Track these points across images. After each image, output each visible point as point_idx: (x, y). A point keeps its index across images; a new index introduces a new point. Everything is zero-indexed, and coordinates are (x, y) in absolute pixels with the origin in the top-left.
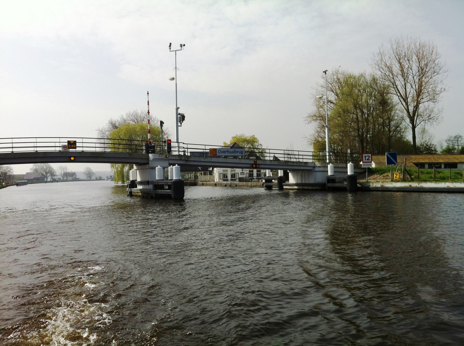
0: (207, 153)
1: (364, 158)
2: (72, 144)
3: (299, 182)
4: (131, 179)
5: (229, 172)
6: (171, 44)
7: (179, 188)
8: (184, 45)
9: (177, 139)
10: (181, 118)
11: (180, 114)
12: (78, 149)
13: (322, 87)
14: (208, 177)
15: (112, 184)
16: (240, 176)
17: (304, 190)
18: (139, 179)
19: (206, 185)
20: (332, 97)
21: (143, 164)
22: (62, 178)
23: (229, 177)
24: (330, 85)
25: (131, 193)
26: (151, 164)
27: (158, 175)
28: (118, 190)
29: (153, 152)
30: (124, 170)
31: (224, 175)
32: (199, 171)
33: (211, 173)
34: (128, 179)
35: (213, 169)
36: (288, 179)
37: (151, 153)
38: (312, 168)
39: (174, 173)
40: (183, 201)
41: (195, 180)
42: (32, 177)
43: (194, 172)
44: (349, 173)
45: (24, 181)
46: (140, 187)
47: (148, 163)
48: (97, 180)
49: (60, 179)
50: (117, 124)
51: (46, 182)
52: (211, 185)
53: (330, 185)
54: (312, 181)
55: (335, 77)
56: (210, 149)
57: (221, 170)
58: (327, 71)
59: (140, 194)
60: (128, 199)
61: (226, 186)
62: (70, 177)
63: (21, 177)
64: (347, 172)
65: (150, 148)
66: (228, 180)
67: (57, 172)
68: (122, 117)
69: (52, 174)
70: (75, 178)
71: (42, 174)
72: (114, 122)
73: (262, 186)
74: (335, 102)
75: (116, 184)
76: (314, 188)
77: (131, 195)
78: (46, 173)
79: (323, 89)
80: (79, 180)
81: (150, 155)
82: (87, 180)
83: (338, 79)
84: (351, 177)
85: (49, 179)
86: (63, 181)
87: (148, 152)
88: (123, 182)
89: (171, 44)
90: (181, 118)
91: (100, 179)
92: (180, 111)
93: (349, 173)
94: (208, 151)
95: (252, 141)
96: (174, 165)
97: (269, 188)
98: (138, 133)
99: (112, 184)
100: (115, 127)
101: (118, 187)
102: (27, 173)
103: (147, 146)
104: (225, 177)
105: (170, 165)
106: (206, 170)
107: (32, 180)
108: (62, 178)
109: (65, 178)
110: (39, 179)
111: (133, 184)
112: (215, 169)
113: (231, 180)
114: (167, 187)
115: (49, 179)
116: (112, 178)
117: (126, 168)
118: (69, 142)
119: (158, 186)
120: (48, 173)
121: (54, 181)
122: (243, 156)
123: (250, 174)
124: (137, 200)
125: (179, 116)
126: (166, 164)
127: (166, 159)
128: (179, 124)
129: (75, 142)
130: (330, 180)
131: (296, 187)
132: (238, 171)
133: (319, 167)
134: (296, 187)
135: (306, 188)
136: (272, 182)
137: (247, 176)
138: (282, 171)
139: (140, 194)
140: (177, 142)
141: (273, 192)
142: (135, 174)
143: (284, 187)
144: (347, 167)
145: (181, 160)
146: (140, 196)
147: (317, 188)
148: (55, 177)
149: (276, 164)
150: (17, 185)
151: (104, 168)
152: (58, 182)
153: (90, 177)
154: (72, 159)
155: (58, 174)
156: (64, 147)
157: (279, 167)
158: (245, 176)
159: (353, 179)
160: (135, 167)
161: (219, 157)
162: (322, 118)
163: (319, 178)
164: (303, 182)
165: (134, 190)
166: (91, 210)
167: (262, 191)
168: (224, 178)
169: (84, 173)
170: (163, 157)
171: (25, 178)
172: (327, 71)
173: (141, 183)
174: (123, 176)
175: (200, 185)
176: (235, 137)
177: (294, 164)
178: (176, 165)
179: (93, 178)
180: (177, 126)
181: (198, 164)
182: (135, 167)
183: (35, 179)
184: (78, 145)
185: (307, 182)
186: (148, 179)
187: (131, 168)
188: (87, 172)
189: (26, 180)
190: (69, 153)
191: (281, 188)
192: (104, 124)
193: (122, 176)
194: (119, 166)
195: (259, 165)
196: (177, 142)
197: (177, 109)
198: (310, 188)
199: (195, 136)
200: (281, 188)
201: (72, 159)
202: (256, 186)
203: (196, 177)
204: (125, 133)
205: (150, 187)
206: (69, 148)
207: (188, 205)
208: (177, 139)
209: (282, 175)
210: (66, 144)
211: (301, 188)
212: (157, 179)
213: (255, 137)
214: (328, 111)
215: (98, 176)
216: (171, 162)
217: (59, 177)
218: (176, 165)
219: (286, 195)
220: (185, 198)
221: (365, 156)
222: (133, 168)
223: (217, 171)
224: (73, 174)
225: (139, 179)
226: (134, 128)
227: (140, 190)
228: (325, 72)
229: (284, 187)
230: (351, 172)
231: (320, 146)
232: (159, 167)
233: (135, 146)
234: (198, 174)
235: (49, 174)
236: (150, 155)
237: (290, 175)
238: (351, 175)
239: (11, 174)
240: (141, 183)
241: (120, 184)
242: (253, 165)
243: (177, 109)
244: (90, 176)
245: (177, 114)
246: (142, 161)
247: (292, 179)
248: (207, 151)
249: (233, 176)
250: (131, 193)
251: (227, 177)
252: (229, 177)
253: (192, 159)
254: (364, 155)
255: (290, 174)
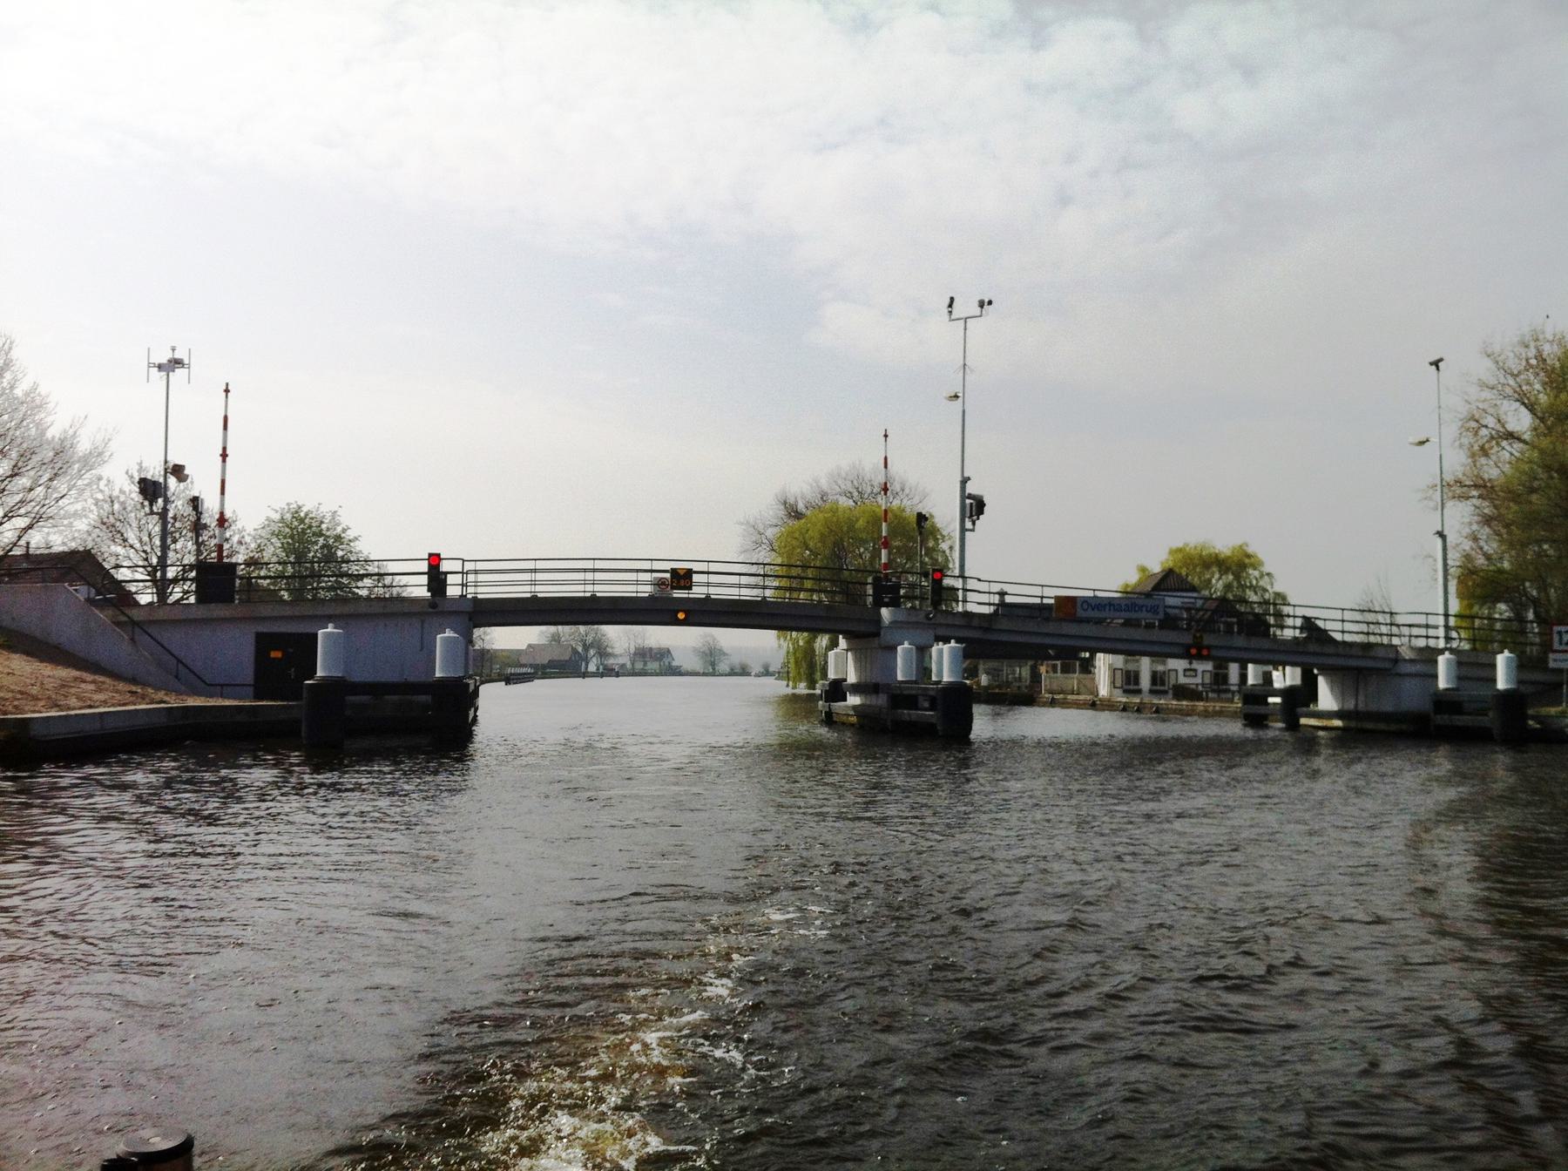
0: (1049, 607)
1: (1556, 638)
2: (682, 578)
3: (1350, 705)
4: (832, 675)
5: (1145, 666)
6: (952, 299)
7: (955, 706)
8: (990, 303)
9: (962, 566)
10: (974, 507)
11: (970, 496)
12: (698, 592)
13: (1483, 385)
14: (1074, 680)
15: (782, 688)
16: (1182, 680)
17: (1365, 733)
18: (852, 678)
19: (1065, 704)
20: (1521, 421)
21: (867, 637)
22: (629, 665)
23: (1145, 682)
24: (1511, 382)
25: (829, 714)
26: (887, 638)
27: (902, 670)
28: (796, 706)
29: (894, 603)
30: (817, 645)
31: (1128, 673)
32: (1049, 658)
33: (1087, 667)
34: (825, 675)
35: (1092, 657)
36: (1314, 697)
37: (887, 605)
38: (1387, 665)
39: (945, 662)
40: (969, 743)
41: (1030, 687)
42: (543, 659)
43: (1030, 663)
44: (1501, 685)
45: (524, 670)
46: (854, 700)
47: (877, 635)
48: (732, 673)
49: (623, 666)
50: (801, 507)
51: (585, 675)
52: (1078, 705)
53: (1442, 719)
54: (1388, 706)
55: (1532, 352)
56: (1057, 598)
57: (1118, 660)
58: (1441, 360)
59: (854, 719)
60: (822, 731)
61: (1124, 710)
62: (656, 663)
63: (513, 657)
64: (1494, 681)
65: (887, 592)
66: (1139, 692)
67: (617, 645)
68: (817, 481)
69: (603, 653)
70: (670, 666)
71: (575, 651)
72: (792, 501)
73: (1233, 715)
74: (1526, 437)
75: (790, 691)
76: (1393, 727)
77: (829, 720)
78: (586, 648)
79: (1487, 394)
80: (681, 674)
81: (885, 612)
82: (704, 674)
83: (1540, 357)
84: (1506, 694)
85: (592, 668)
86: (634, 673)
87: (879, 603)
88: (812, 685)
89: (952, 299)
90: (974, 507)
91: (744, 672)
92: (971, 488)
93: (1501, 685)
94: (1052, 601)
95: (1239, 565)
96: (946, 640)
97: (1256, 722)
98: (864, 536)
99: (782, 688)
100: (794, 513)
101: (795, 698)
102: (530, 646)
103: (877, 584)
104: (1129, 681)
105: (938, 639)
106: (1075, 659)
107: (544, 667)
108: (629, 665)
109: (639, 666)
110: (566, 667)
111: (837, 690)
112: (1100, 656)
113: (1151, 692)
114: (926, 705)
115: (592, 668)
116: (784, 675)
117: (823, 641)
118: (674, 572)
119: (902, 697)
120: (591, 645)
121: (608, 672)
122: (1201, 618)
123: (1216, 675)
124: (849, 737)
125: (968, 501)
126: (924, 636)
127: (928, 623)
128: (968, 525)
129: (690, 572)
130: (1444, 703)
131: (1338, 723)
132: (1177, 664)
133: (1411, 661)
134: (1338, 723)
135: (1370, 726)
136: (1267, 704)
137: (1207, 681)
138: (1298, 670)
139: (854, 719)
140: (962, 576)
141: (1270, 734)
142: (842, 663)
143: (1303, 721)
144: (1493, 666)
145: (968, 627)
146: (853, 725)
147: (1404, 727)
148: (611, 661)
149: (1316, 648)
150: (509, 680)
151: (763, 644)
152: (617, 675)
153: (713, 664)
154: (681, 616)
155: (617, 651)
156: (660, 583)
157: (1251, 655)
158: (1198, 680)
159: (1511, 702)
160: (843, 643)
161: (1081, 621)
162: (1485, 489)
163: (1410, 697)
164: (1361, 707)
165: (838, 706)
166: (727, 750)
167: (1234, 729)
168: (1128, 683)
169: (695, 650)
170: (921, 617)
171: (523, 661)
172: (1441, 360)
173: (857, 689)
174: (812, 666)
175: (1044, 705)
176: (1179, 550)
177: (1354, 651)
178: (953, 643)
179: (723, 667)
180: (963, 530)
181: (1038, 641)
182: (843, 643)
183: (552, 664)
184: (696, 578)
185: (1373, 707)
186: (877, 678)
187: (834, 644)
188: (705, 649)
189: (531, 666)
190: (673, 600)
191: (1293, 725)
192: (763, 507)
193: (809, 665)
194: (801, 638)
195: (1209, 648)
196: (962, 576)
197: (965, 481)
198: (1382, 726)
199: (1002, 565)
200: (1293, 725)
201: (681, 616)
202: (1219, 714)
203: (1036, 677)
204: (822, 535)
205: (881, 700)
206: (673, 588)
207: (979, 757)
208: (962, 566)
209: (1298, 681)
210: (668, 575)
211: (1353, 724)
212: (900, 678)
213: (1250, 550)
214: (1501, 465)
215: (736, 660)
216: (941, 632)
217: (621, 661)
218: (953, 643)
219: (1307, 744)
220: (972, 736)
221: (1560, 633)
222: (837, 645)
223: (1104, 663)
224: (662, 654)
225: (852, 678)
226: (851, 524)
227: (854, 708)
228: (1436, 364)
229: (1303, 721)
230: (1507, 681)
231: (1480, 586)
232: (906, 645)
233: (854, 577)
234: (1043, 669)
235: (592, 652)
236: (885, 612)
237: (1323, 686)
238: (1506, 691)
239: (487, 647)
240: (857, 689)
241: (802, 689)
242: (1188, 647)
243: (965, 481)
244: (712, 665)
245: (964, 496)
246: (862, 628)
247: (1326, 699)
248: (1046, 601)
249: (1156, 678)
250: (829, 714)
251: (1137, 682)
252: (1145, 682)
253: (1004, 624)
254: (1556, 628)
255: (1321, 681)
